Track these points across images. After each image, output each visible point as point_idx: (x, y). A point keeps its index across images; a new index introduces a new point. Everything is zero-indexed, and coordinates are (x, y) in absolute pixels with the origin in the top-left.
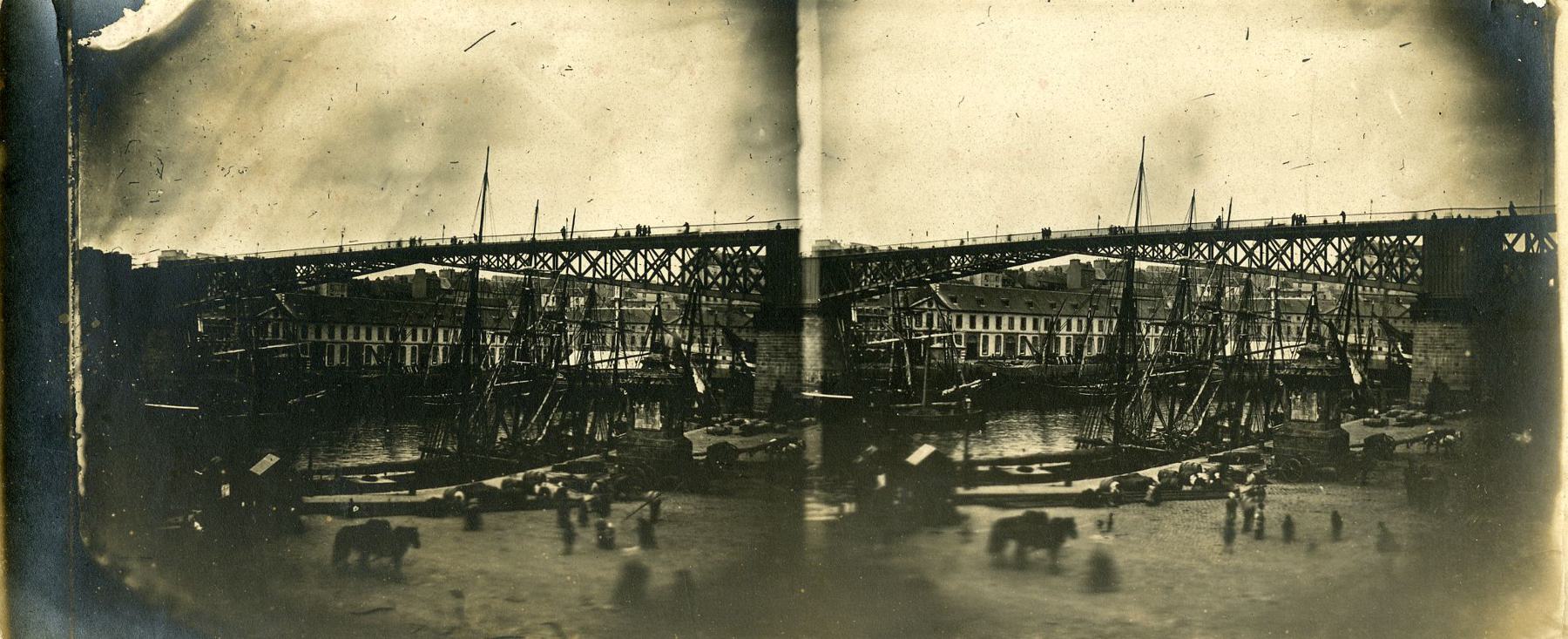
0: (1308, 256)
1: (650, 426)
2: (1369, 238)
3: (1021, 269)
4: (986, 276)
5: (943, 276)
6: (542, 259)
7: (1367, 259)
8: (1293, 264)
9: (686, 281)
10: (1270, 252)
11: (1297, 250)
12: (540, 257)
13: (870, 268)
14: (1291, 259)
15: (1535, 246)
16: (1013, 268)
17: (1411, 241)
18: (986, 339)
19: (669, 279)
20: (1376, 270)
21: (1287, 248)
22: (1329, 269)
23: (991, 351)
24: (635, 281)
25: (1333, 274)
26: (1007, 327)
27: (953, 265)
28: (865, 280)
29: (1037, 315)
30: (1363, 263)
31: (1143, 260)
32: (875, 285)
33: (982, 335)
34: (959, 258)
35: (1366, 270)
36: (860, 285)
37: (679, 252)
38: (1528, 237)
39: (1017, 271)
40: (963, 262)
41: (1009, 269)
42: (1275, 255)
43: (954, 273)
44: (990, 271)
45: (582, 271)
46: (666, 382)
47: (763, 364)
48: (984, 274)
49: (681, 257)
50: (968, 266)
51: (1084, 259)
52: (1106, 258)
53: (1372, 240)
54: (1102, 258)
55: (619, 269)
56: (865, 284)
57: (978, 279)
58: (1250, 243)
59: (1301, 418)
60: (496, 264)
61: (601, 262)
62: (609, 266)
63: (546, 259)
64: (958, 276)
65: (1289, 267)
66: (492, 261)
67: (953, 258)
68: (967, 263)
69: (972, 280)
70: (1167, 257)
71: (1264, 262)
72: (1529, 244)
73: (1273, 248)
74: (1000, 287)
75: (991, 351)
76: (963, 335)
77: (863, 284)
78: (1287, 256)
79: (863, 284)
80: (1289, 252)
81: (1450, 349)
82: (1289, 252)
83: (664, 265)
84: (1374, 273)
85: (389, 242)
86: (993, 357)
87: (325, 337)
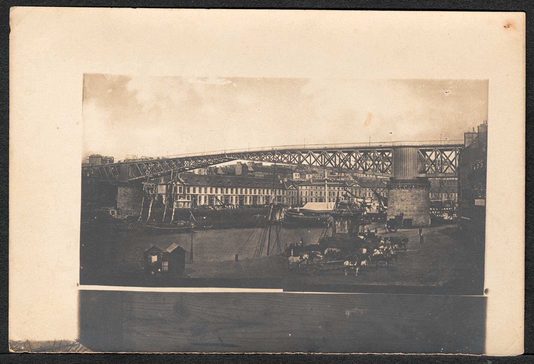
0: (342, 161)
1: (343, 232)
2: (369, 153)
3: (215, 167)
4: (200, 170)
5: (181, 170)
6: (293, 157)
7: (368, 162)
8: (336, 164)
9: (357, 168)
10: (326, 159)
11: (337, 158)
12: (292, 156)
13: (150, 167)
14: (335, 162)
15: (439, 157)
16: (212, 166)
17: (387, 155)
18: (200, 197)
19: (350, 166)
20: (372, 167)
21: (333, 157)
22: (351, 167)
23: (203, 203)
24: (335, 167)
25: (353, 169)
26: (209, 192)
27: (186, 165)
28: (148, 172)
29: (321, 186)
30: (366, 164)
31: (269, 162)
32: (152, 174)
33: (198, 196)
34: (188, 162)
35: (368, 167)
36: (145, 174)
37: (354, 154)
38: (436, 153)
39: (213, 167)
40: (190, 164)
41: (210, 166)
42: (328, 160)
43: (186, 169)
44: (202, 167)
45: (312, 163)
46: (349, 212)
47: (391, 204)
48: (199, 169)
49: (355, 157)
50: (192, 166)
51: (243, 162)
52: (252, 161)
53: (370, 154)
54: (251, 161)
55: (328, 162)
56: (148, 174)
57: (196, 171)
58: (317, 155)
59: (340, 232)
60: (273, 159)
61: (320, 159)
62: (323, 160)
63: (295, 157)
64: (188, 170)
65: (334, 166)
66: (271, 158)
67: (185, 162)
68: (192, 164)
69: (194, 171)
70: (280, 160)
71: (323, 164)
72: (436, 156)
73: (327, 157)
74: (206, 174)
75: (203, 203)
76: (252, 197)
77: (147, 174)
78: (333, 161)
79: (147, 174)
80: (334, 159)
81: (404, 201)
82: (334, 159)
83: (348, 160)
84: (370, 169)
85: (225, 150)
86: (203, 206)
87: (197, 192)
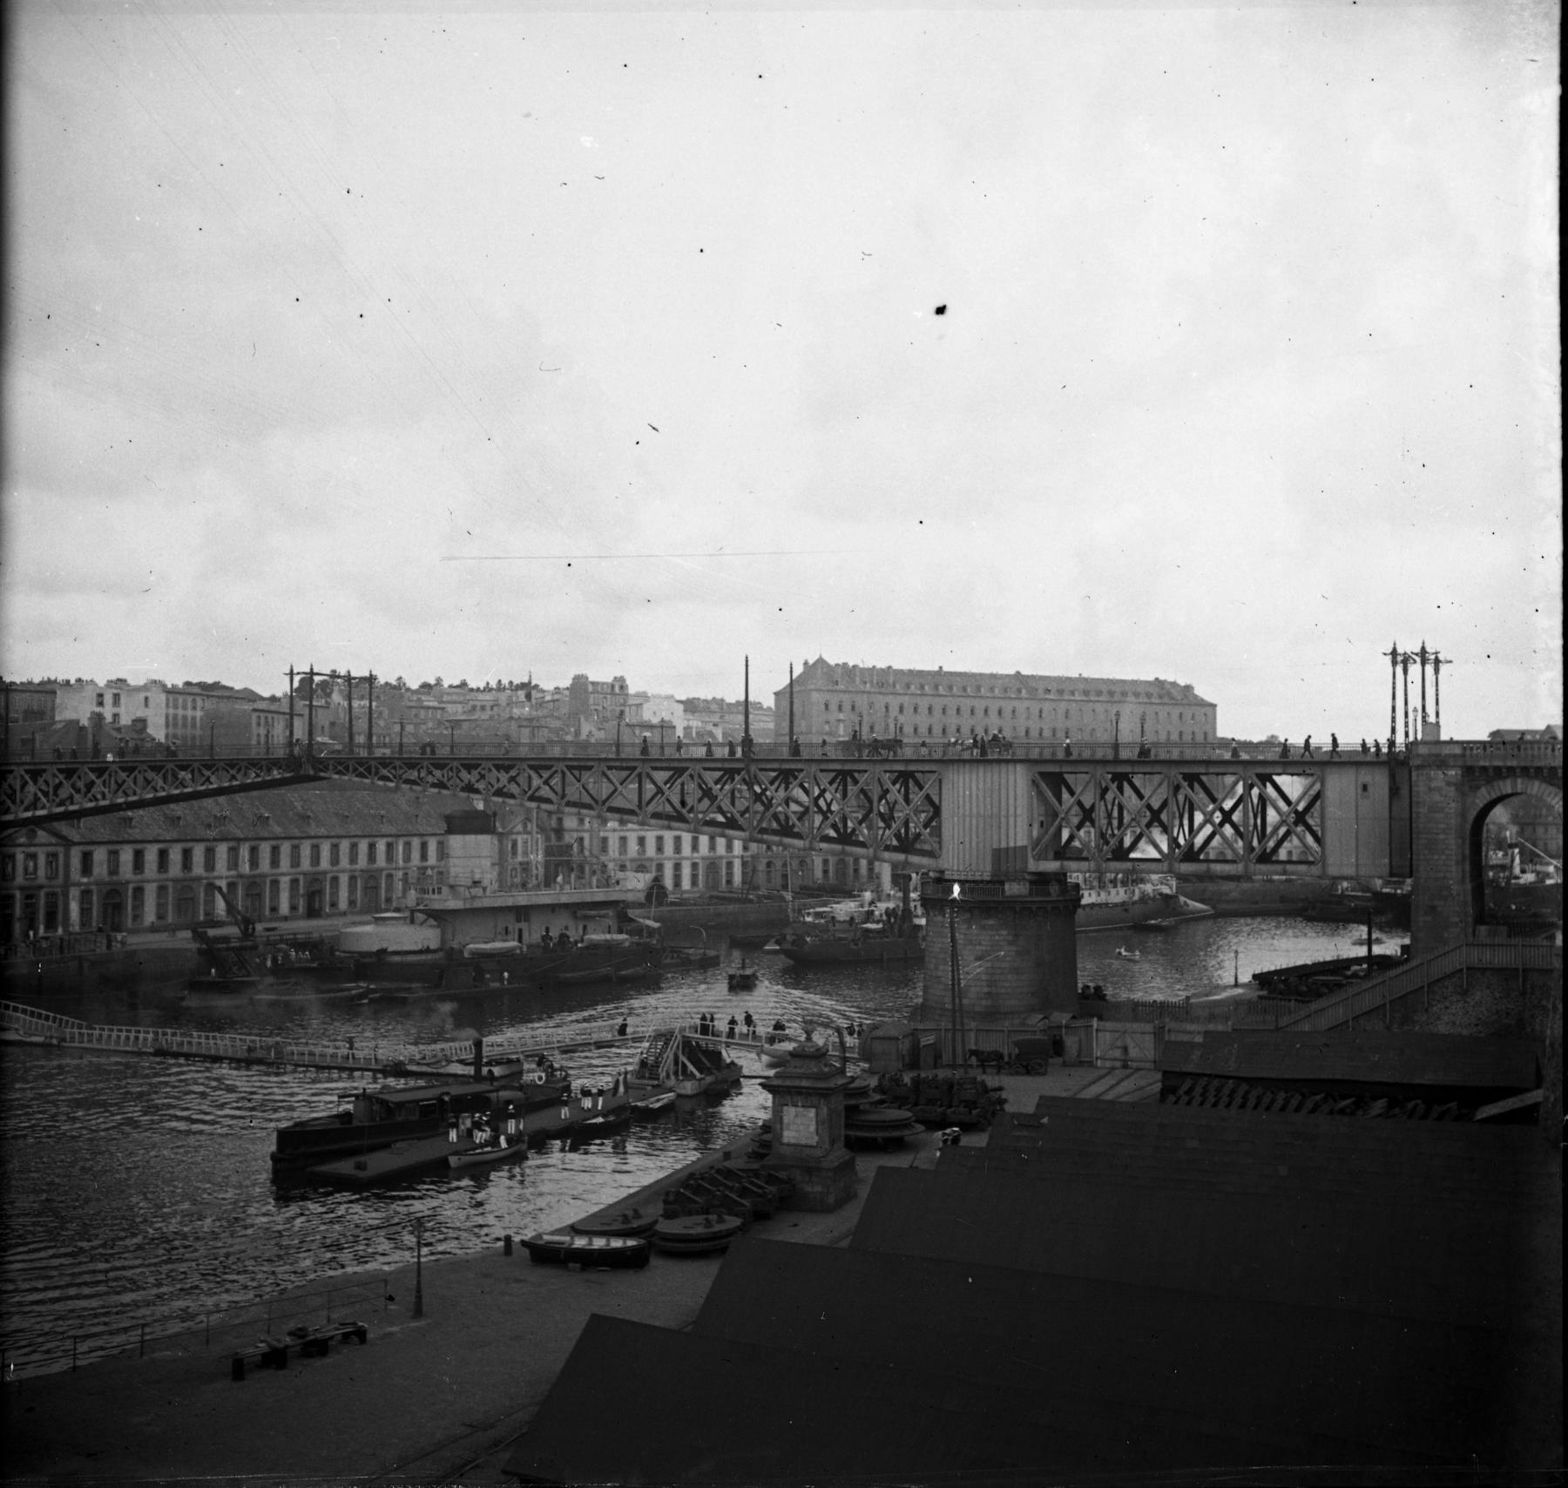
18: (275, 883)
33: (329, 876)
